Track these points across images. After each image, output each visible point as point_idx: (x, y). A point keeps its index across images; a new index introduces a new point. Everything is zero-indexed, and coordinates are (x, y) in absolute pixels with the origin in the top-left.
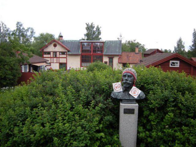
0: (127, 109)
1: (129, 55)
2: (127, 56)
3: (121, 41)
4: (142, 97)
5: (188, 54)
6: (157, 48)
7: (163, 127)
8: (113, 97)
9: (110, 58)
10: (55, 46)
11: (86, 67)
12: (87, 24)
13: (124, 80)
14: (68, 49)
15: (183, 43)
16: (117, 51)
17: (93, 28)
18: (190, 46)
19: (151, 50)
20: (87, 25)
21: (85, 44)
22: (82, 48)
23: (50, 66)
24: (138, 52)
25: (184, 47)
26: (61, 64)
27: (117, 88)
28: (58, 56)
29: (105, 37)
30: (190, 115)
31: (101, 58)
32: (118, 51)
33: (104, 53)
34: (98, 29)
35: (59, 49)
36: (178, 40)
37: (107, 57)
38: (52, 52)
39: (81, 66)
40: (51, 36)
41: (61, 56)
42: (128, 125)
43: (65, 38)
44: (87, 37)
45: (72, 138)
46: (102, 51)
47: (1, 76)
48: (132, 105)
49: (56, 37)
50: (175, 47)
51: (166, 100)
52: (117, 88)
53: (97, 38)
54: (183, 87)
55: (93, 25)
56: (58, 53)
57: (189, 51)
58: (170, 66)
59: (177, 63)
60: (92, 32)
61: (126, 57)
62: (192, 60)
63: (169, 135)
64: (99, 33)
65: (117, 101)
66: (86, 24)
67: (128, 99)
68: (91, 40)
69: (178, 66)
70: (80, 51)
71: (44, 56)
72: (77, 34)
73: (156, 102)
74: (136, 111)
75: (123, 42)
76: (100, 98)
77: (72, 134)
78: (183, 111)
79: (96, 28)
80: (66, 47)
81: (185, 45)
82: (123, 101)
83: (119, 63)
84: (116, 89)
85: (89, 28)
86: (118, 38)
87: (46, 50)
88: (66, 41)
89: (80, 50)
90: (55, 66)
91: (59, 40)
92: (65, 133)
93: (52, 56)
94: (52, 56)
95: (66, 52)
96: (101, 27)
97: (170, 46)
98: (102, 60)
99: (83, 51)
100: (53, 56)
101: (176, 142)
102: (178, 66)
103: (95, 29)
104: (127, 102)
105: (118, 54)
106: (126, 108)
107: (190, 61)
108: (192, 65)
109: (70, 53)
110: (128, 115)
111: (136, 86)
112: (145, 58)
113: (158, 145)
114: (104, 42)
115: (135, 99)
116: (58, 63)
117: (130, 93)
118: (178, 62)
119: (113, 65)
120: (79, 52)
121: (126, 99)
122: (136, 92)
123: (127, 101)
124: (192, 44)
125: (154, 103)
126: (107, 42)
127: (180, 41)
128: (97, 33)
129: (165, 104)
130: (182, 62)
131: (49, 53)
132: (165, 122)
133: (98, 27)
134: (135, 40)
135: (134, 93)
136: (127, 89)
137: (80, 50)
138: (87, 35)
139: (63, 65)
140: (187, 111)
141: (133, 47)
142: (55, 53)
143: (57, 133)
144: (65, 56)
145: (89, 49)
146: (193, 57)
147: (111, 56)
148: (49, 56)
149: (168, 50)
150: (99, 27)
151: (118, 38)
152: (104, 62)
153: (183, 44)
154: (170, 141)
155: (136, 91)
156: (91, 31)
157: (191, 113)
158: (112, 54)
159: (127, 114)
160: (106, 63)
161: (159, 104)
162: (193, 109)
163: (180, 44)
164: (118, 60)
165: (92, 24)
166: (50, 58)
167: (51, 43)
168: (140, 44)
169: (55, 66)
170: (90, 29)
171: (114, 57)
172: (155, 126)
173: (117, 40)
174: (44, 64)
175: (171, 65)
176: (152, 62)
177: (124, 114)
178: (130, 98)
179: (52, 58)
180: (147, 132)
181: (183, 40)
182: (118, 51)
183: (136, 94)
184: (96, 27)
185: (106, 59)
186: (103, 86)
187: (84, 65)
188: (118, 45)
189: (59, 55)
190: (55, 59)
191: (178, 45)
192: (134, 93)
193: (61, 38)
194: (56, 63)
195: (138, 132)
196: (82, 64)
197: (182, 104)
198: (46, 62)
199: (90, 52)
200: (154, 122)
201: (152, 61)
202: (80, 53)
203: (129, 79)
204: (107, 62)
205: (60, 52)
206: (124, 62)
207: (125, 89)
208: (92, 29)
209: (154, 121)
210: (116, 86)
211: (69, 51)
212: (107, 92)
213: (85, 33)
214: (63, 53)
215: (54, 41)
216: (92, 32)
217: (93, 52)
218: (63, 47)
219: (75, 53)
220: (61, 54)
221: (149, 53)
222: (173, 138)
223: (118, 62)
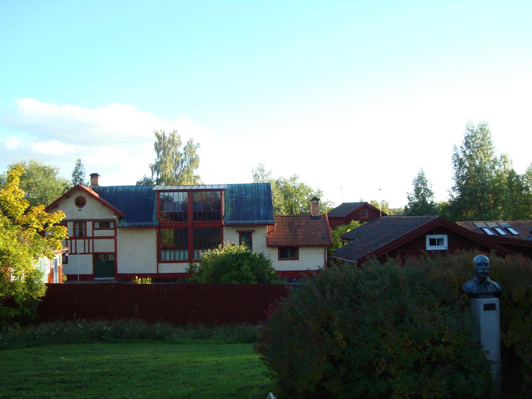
1: (296, 224)
8: (468, 291)
10: (80, 203)
12: (160, 134)
28: (89, 234)
34: (190, 148)
39: (160, 260)
41: (97, 233)
47: (1, 297)
56: (89, 225)
58: (429, 248)
66: (157, 135)
95: (113, 221)
103: (181, 150)
106: (486, 303)
110: (488, 312)
116: (89, 253)
118: (445, 237)
127: (421, 180)
134: (294, 179)
144: (111, 233)
150: (194, 143)
163: (421, 187)
171: (254, 231)
181: (427, 177)
184: (184, 144)
188: (262, 197)
189: (94, 229)
190: (80, 242)
191: (418, 190)
194: (85, 253)
205: (94, 221)
214: (104, 224)
217: (194, 220)
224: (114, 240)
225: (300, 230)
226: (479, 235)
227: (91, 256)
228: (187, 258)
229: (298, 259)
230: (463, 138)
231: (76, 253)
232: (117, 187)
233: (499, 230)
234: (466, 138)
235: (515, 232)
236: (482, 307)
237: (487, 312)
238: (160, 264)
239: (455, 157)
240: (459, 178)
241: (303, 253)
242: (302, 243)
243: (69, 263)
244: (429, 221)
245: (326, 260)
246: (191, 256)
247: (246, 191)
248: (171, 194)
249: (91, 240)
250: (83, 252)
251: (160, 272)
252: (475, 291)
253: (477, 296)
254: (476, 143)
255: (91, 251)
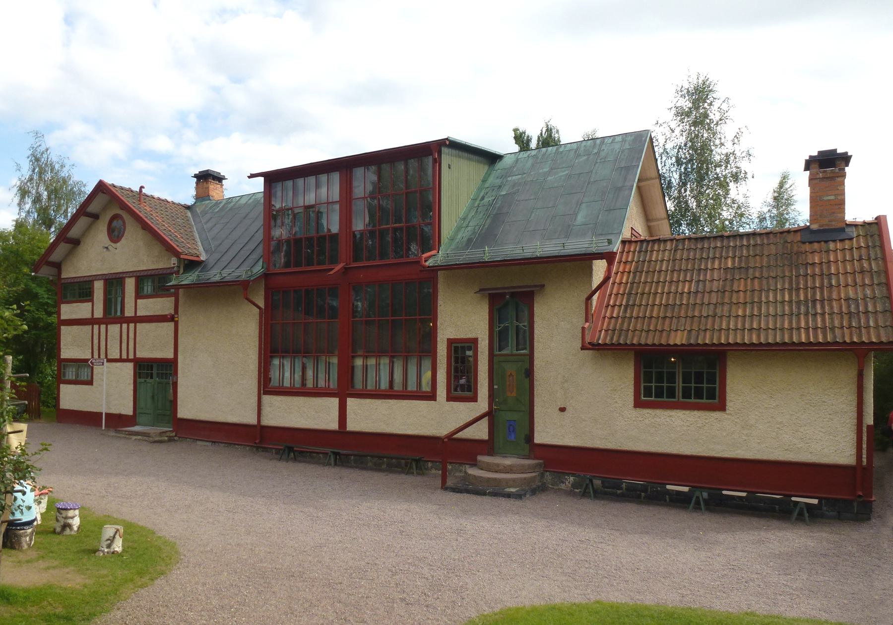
28: (129, 312)
56: (130, 285)
189: (139, 295)
194: (120, 360)
205: (141, 278)
224: (172, 324)
227: (130, 366)
228: (334, 384)
229: (638, 404)
241: (739, 384)
243: (479, 399)
245: (869, 420)
246: (347, 373)
249: (132, 325)
250: (118, 357)
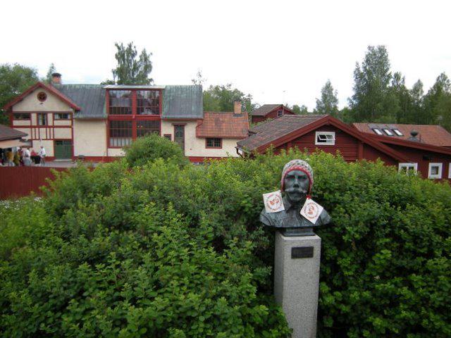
0: (298, 248)
1: (221, 120)
2: (217, 122)
3: (200, 87)
4: (324, 219)
5: (345, 115)
6: (281, 104)
7: (368, 279)
8: (267, 223)
9: (176, 127)
10: (42, 98)
11: (126, 148)
12: (119, 45)
13: (290, 187)
14: (76, 105)
15: (333, 92)
16: (193, 109)
17: (134, 55)
18: (349, 99)
19: (266, 107)
20: (119, 48)
21: (120, 94)
22: (110, 103)
23: (32, 147)
24: (240, 112)
25: (336, 101)
26: (58, 142)
27: (274, 203)
28: (50, 123)
29: (160, 78)
30: (422, 251)
31: (155, 125)
32: (195, 111)
33: (163, 116)
34: (145, 57)
35: (51, 105)
36: (325, 85)
37: (171, 124)
38: (33, 112)
39: (109, 146)
40: (29, 73)
41: (57, 123)
42: (300, 284)
43: (67, 79)
44: (120, 76)
45: (208, 326)
46: (157, 111)
48: (297, 238)
49: (42, 75)
50: (318, 100)
51: (372, 224)
52: (274, 203)
53: (143, 78)
54: (399, 196)
55: (133, 48)
56: (50, 116)
57: (346, 109)
58: (317, 143)
59: (330, 137)
60: (131, 65)
61: (214, 124)
62: (354, 127)
63: (385, 295)
64: (148, 68)
65: (274, 231)
66: (116, 45)
67: (299, 226)
68: (128, 84)
69: (333, 144)
70: (105, 110)
71: (14, 125)
72: (91, 68)
73: (355, 229)
74: (317, 252)
75: (205, 88)
76: (240, 227)
77: (208, 315)
78: (407, 244)
79: (140, 57)
80: (69, 101)
81: (338, 97)
82: (287, 231)
83: (199, 137)
84: (271, 206)
85: (124, 55)
86: (193, 81)
87: (19, 108)
88: (70, 86)
89: (105, 105)
90: (46, 149)
91: (49, 82)
92: (193, 316)
93: (34, 123)
94: (34, 123)
95: (71, 113)
96: (151, 54)
97: (309, 101)
98: (159, 131)
99: (112, 110)
100: (38, 122)
101: (401, 306)
102: (333, 144)
104: (295, 233)
105: (195, 116)
106: (296, 245)
107: (412, 139)
108: (360, 141)
109: (81, 116)
111: (314, 199)
112: (253, 127)
113: (325, 318)
114: (164, 89)
115: (311, 225)
116: (50, 139)
117: (302, 213)
118: (333, 134)
119: (183, 142)
120: (102, 112)
121: (295, 226)
122: (313, 211)
123: (296, 230)
124: (353, 93)
125: (353, 233)
126: (169, 88)
128: (141, 69)
129: (371, 233)
130: (341, 133)
131: (27, 116)
132: (373, 269)
133: (144, 53)
134: (230, 85)
135: (310, 213)
136: (294, 205)
137: (105, 105)
138: (120, 72)
139: (63, 147)
140: (415, 243)
141: (226, 101)
142: (43, 115)
143: (173, 318)
144: (68, 123)
145: (127, 105)
146: (356, 122)
147: (177, 123)
148: (27, 123)
149: (300, 106)
150: (148, 53)
151: (193, 81)
152: (162, 135)
153: (334, 95)
154: (384, 306)
155: (313, 209)
156: (129, 62)
157: (423, 247)
158: (179, 117)
159: (297, 260)
160: (168, 136)
161: (361, 233)
162: (428, 238)
164: (197, 130)
165: (130, 46)
166: (31, 127)
167: (30, 92)
168: (242, 95)
169: (46, 149)
170: (126, 57)
171: (186, 124)
172: (351, 278)
173: (192, 84)
174: (15, 145)
175: (319, 141)
176: (276, 135)
177: (293, 260)
178: (303, 225)
179: (35, 127)
180: (338, 293)
182: (195, 111)
183: (314, 214)
184: (139, 53)
185: (167, 129)
186: (244, 202)
187: (123, 145)
188: (195, 96)
189: (54, 119)
190: (43, 130)
191: (325, 96)
192: (310, 213)
193: (55, 79)
195: (321, 295)
196: (111, 140)
197: (406, 230)
198: (20, 138)
199: (131, 113)
200: (348, 270)
201: (276, 133)
202: (105, 114)
203: (302, 184)
204: (171, 135)
205: (54, 113)
206: (210, 135)
207: (290, 205)
208: (130, 58)
209: (349, 268)
210: (271, 199)
211: (77, 111)
212: (251, 216)
213: (115, 68)
214: (63, 116)
215: (40, 85)
216: (131, 65)
218: (62, 100)
219: (94, 116)
220: (57, 117)
221: (263, 114)
222: (390, 299)
223: (197, 134)
225: (224, 124)
226: (370, 135)
230: (364, 56)
231: (39, 139)
232: (75, 85)
233: (387, 131)
234: (367, 56)
235: (399, 134)
236: (288, 253)
237: (297, 260)
238: (109, 149)
239: (357, 72)
240: (359, 89)
241: (225, 143)
242: (224, 135)
244: (320, 119)
247: (182, 92)
248: (114, 92)
249: (52, 129)
251: (109, 155)
252: (280, 224)
253: (283, 230)
254: (377, 60)
255: (52, 138)
